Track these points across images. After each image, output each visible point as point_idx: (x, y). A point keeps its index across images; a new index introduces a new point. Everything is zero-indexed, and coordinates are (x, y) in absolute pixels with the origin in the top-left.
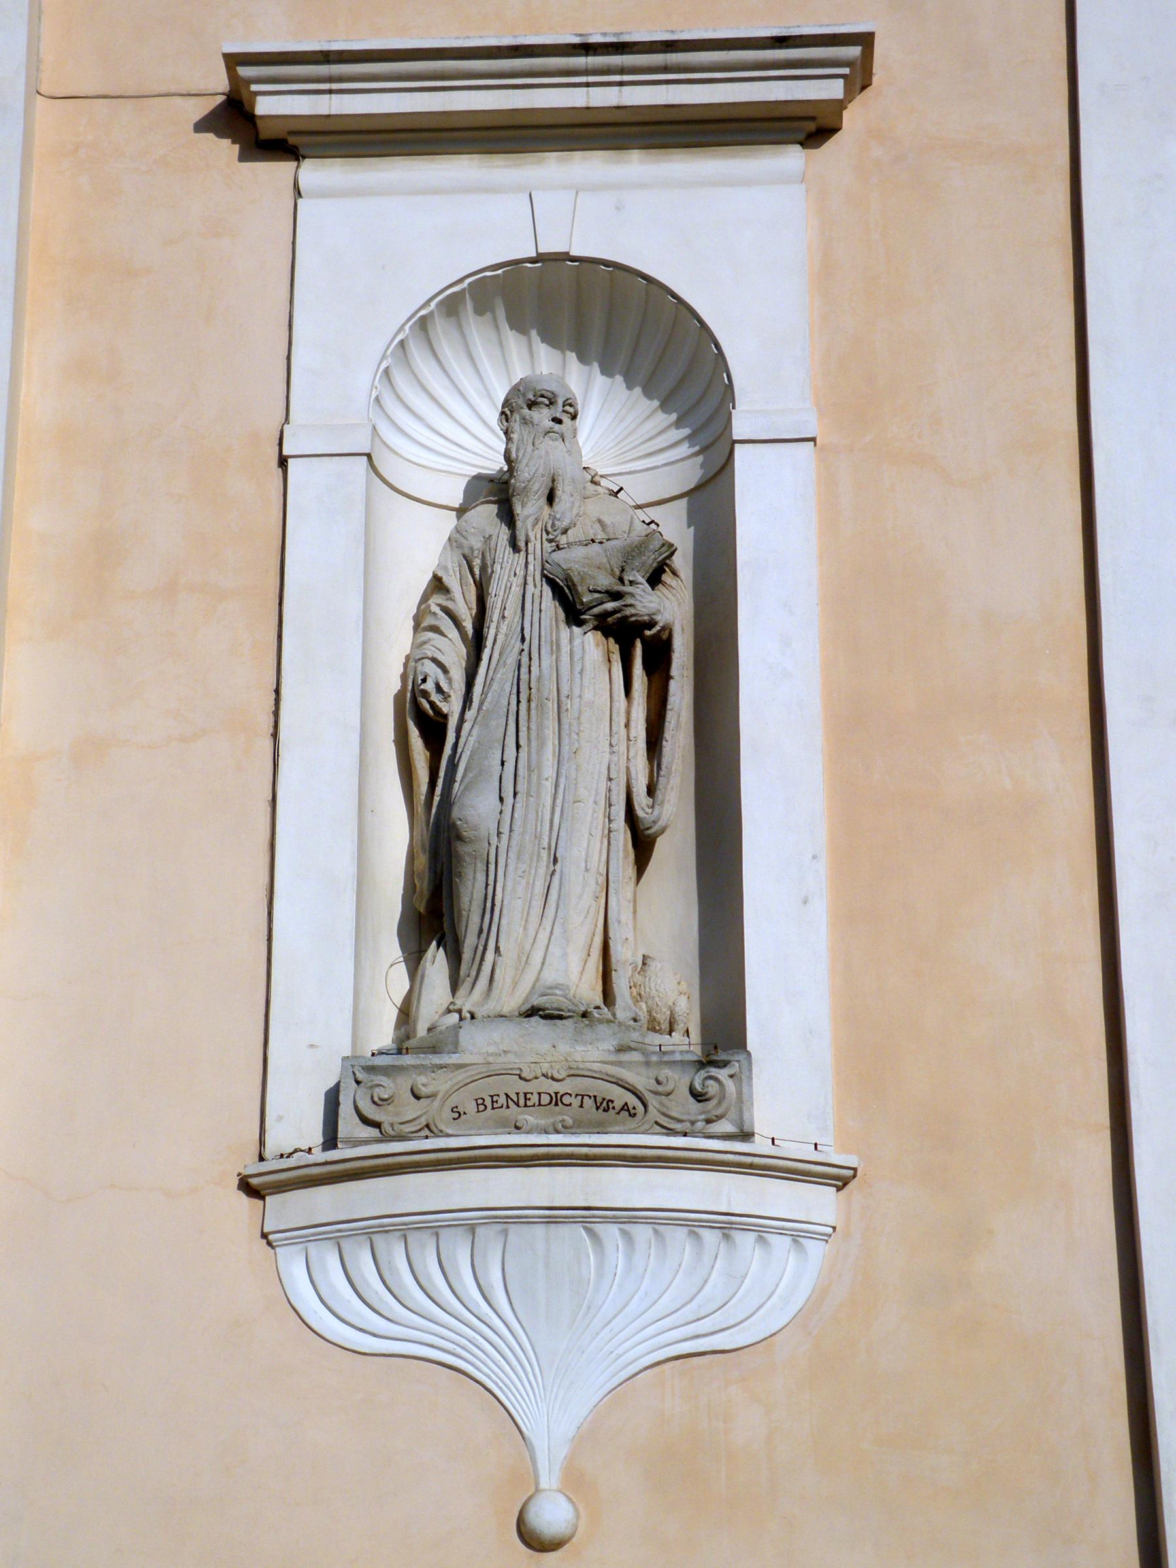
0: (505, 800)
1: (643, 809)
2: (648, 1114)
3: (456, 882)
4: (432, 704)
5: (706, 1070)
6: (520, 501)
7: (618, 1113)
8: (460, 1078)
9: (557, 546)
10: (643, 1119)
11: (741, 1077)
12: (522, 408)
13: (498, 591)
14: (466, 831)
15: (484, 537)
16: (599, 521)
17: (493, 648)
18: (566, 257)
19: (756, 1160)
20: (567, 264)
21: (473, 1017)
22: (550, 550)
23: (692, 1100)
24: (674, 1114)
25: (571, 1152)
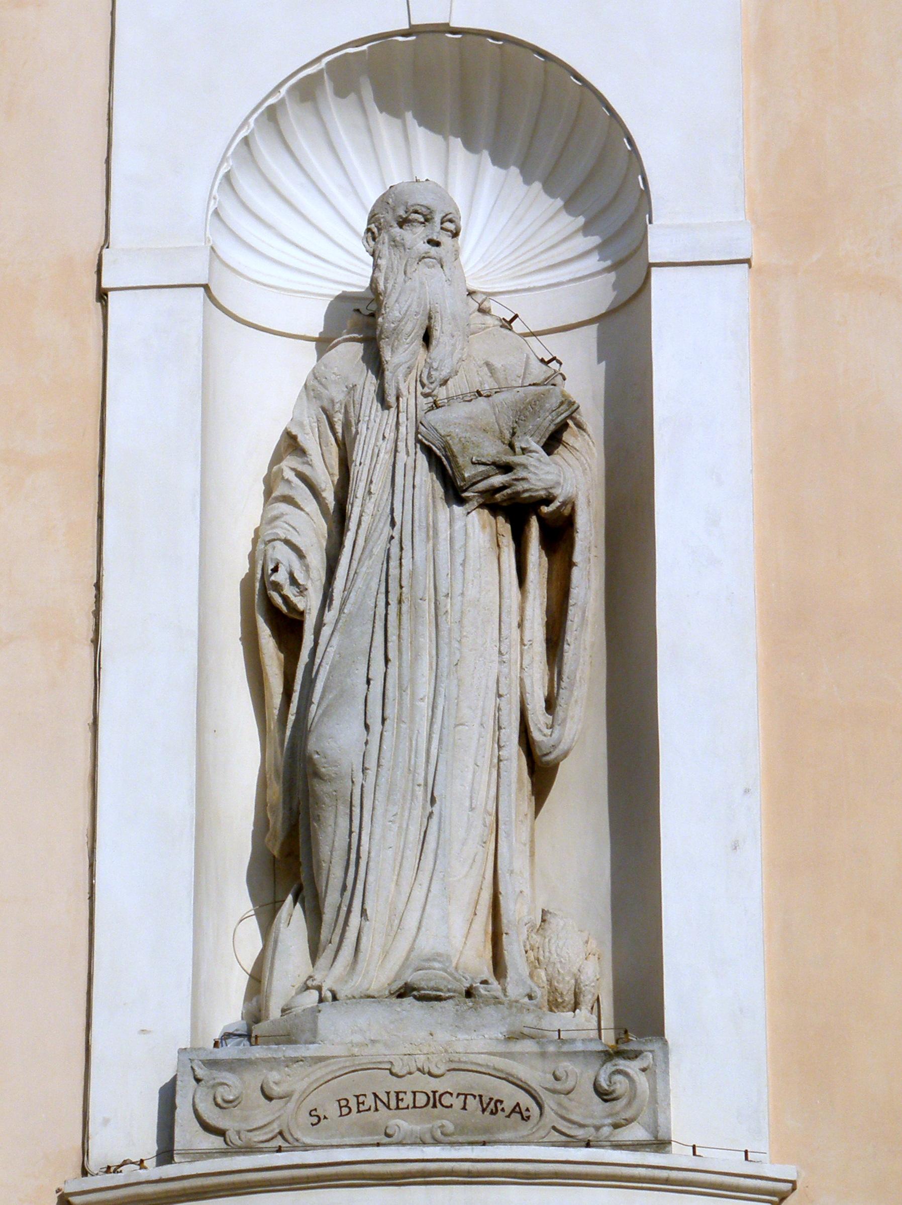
0: (371, 727)
1: (540, 730)
2: (543, 1118)
3: (314, 826)
4: (285, 599)
5: (614, 1062)
6: (389, 345)
7: (509, 1116)
8: (319, 1074)
9: (435, 402)
10: (538, 1123)
11: (655, 1072)
12: (391, 226)
13: (363, 458)
14: (324, 767)
15: (347, 387)
16: (488, 364)
17: (357, 533)
18: (446, 28)
19: (674, 1175)
20: (446, 36)
21: (335, 998)
22: (426, 407)
23: (597, 1099)
24: (574, 1117)
25: (450, 1168)
